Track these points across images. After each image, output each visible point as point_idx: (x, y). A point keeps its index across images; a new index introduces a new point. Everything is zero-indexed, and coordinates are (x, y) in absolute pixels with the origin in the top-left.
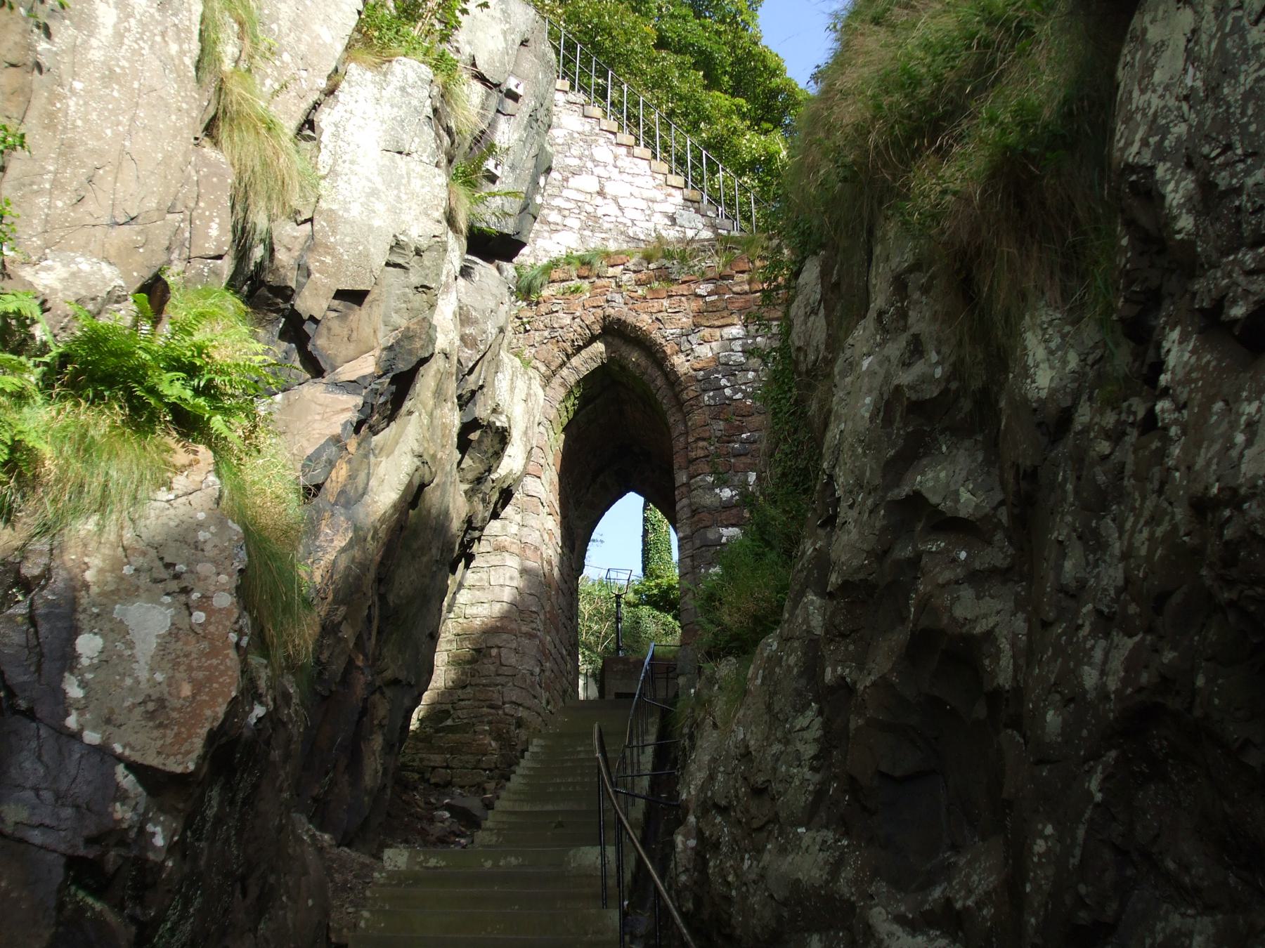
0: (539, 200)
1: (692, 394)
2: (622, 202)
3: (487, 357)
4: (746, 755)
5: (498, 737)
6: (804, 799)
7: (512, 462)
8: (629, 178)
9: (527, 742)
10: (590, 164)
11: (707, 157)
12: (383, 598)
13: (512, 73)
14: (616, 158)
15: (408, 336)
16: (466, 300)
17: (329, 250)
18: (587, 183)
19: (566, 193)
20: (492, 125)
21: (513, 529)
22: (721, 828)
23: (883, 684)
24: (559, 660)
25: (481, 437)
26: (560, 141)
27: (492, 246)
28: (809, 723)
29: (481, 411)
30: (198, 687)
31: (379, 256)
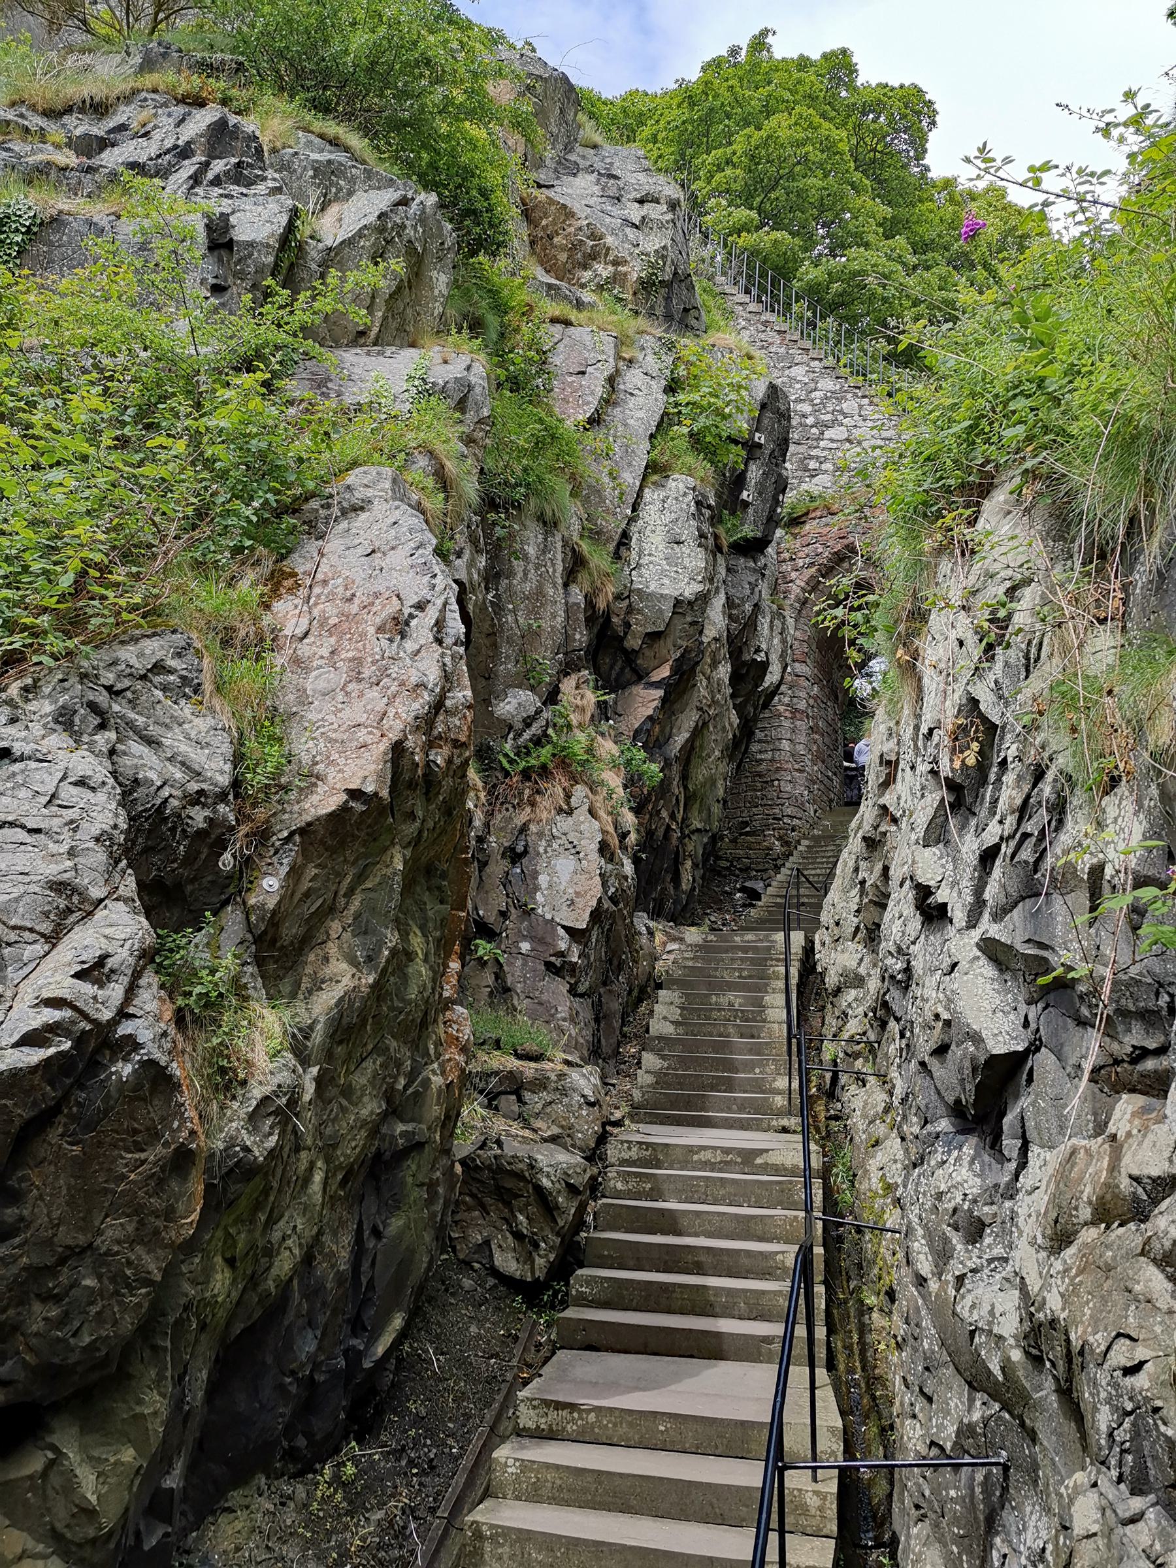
3: (751, 624)
5: (780, 839)
8: (870, 424)
9: (798, 842)
10: (840, 418)
14: (861, 407)
16: (732, 591)
17: (639, 612)
19: (822, 444)
21: (786, 700)
24: (826, 781)
25: (747, 674)
26: (817, 401)
29: (746, 657)
31: (667, 608)
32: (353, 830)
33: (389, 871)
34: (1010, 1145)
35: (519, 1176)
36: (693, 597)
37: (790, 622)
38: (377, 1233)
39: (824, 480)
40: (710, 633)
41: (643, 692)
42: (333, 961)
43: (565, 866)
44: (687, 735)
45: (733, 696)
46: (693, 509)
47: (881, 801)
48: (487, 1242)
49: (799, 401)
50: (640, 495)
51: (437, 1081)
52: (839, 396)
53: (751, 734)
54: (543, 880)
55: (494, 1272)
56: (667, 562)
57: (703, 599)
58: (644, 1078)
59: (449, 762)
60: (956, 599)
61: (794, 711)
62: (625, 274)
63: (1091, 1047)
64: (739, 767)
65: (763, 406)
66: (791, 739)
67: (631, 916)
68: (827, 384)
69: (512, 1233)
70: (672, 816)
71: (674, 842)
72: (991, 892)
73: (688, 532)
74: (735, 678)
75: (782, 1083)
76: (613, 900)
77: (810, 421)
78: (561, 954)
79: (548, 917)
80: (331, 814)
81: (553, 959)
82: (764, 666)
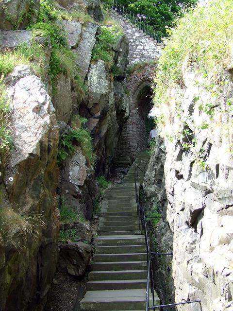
2: (148, 51)
3: (121, 100)
6: (153, 181)
14: (146, 41)
15: (105, 108)
16: (115, 91)
17: (91, 98)
18: (141, 47)
19: (137, 50)
25: (120, 113)
29: (120, 109)
30: (82, 176)
32: (31, 163)
34: (199, 230)
35: (73, 250)
37: (131, 98)
38: (42, 265)
39: (137, 60)
40: (111, 102)
41: (93, 120)
42: (27, 198)
43: (76, 169)
44: (105, 131)
45: (117, 119)
46: (104, 70)
47: (160, 148)
48: (66, 267)
49: (130, 39)
50: (90, 66)
51: (55, 227)
52: (140, 38)
53: (122, 129)
54: (71, 173)
55: (69, 274)
56: (97, 82)
57: (108, 94)
58: (101, 224)
59: (54, 144)
61: (133, 123)
62: (83, 6)
63: (218, 205)
64: (119, 138)
65: (122, 41)
66: (132, 130)
67: (94, 181)
68: (137, 34)
70: (103, 154)
71: (103, 160)
72: (194, 172)
73: (104, 76)
74: (117, 114)
75: (137, 222)
76: (89, 177)
77: (133, 44)
78: (77, 193)
79: (73, 183)
80: (25, 160)
81: (75, 194)
82: (125, 111)
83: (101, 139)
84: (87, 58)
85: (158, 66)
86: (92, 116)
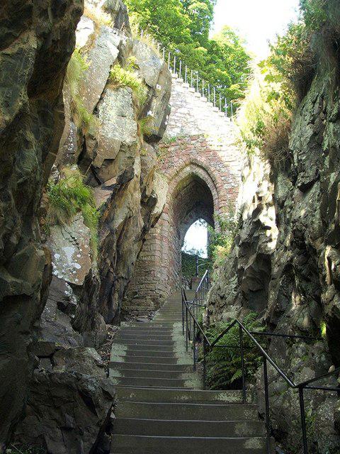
0: (166, 123)
1: (220, 185)
4: (219, 289)
5: (153, 300)
7: (157, 210)
10: (184, 104)
11: (15, 445)
12: (118, 251)
13: (157, 83)
15: (126, 172)
19: (177, 114)
20: (151, 101)
22: (212, 308)
23: (250, 268)
25: (148, 202)
27: (153, 139)
28: (234, 280)
31: (117, 148)
33: (25, 47)
35: (68, 387)
36: (131, 144)
48: (42, 437)
50: (104, 93)
54: (57, 256)
60: (103, 372)
69: (61, 428)
78: (68, 299)
82: (155, 201)
83: (112, 233)
84: (100, 76)
85: (252, 65)
86: (100, 184)
